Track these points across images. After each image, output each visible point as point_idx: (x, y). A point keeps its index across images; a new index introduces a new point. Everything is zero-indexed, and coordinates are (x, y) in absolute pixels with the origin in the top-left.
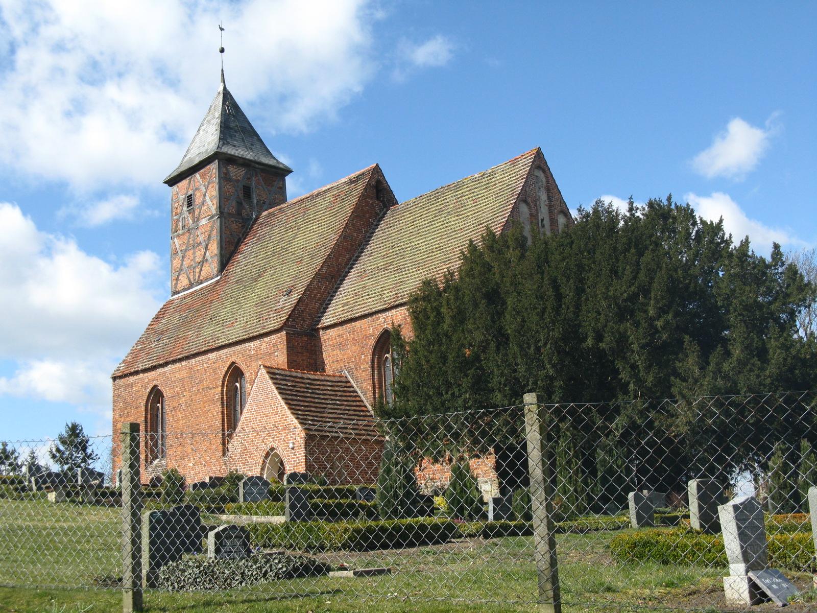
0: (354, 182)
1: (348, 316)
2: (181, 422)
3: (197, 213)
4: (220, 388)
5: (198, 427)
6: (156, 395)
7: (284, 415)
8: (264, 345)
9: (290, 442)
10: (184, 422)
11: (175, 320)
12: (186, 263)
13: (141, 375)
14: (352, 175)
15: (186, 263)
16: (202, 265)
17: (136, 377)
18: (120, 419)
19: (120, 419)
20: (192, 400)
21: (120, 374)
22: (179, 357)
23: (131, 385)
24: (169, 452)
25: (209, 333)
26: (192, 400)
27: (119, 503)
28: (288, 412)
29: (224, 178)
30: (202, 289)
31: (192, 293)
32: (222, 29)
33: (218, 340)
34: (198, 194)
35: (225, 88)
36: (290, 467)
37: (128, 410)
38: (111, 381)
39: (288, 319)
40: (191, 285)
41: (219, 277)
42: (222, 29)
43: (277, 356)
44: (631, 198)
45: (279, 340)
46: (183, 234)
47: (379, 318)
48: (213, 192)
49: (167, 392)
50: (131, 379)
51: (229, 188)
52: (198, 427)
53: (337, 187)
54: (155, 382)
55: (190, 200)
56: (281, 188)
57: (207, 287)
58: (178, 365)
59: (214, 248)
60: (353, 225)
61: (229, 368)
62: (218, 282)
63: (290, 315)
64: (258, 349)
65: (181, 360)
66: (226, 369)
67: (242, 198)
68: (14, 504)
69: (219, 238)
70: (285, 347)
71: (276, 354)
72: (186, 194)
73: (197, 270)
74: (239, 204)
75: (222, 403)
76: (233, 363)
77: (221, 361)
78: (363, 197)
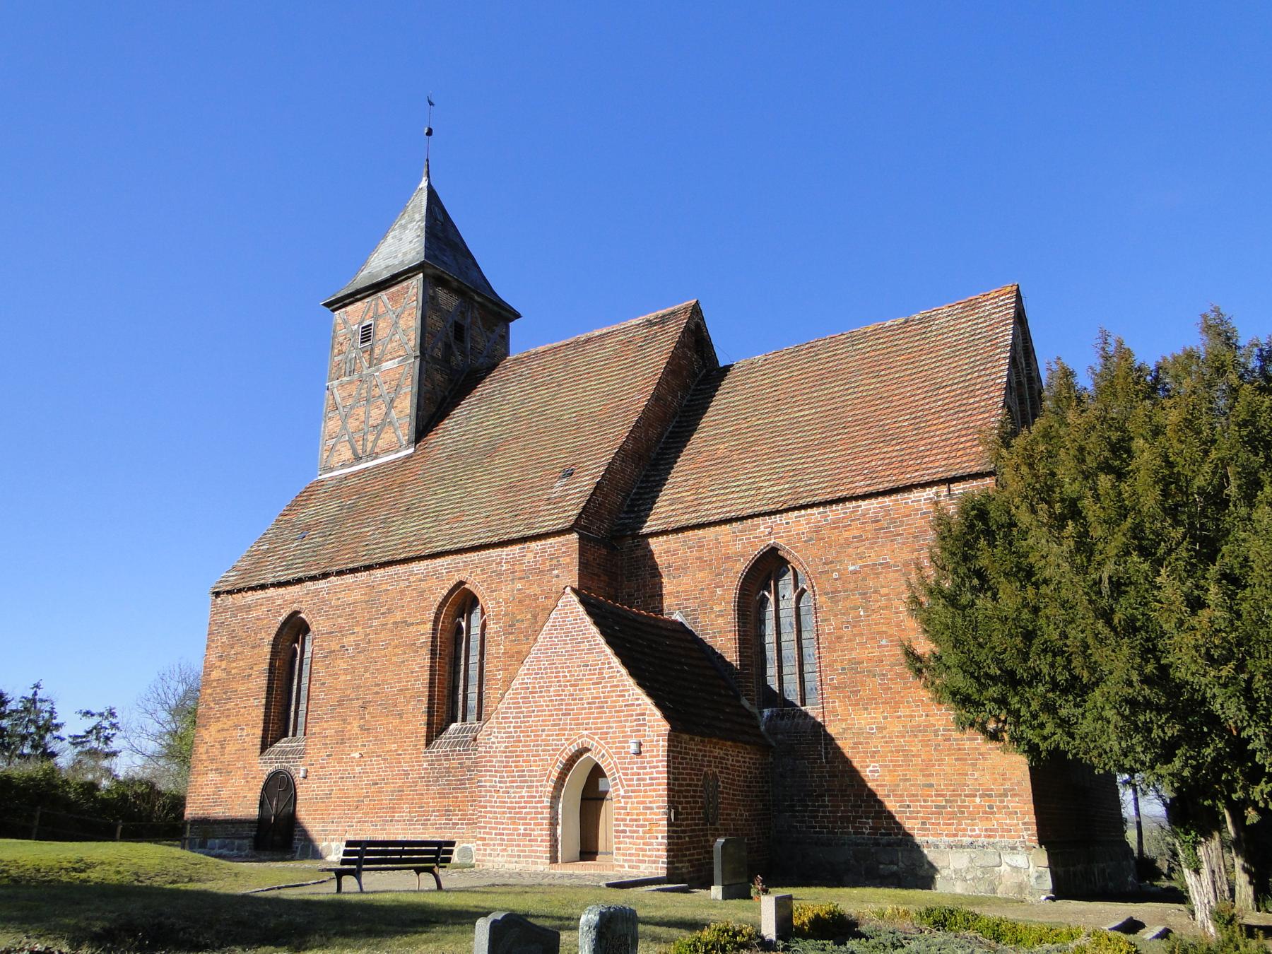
0: (655, 324)
1: (684, 520)
2: (342, 678)
3: (377, 351)
4: (430, 625)
5: (376, 689)
6: (295, 628)
7: (617, 686)
8: (530, 555)
9: (631, 740)
10: (349, 677)
11: (333, 507)
12: (352, 424)
13: (271, 591)
14: (651, 316)
15: (352, 424)
16: (382, 430)
17: (260, 594)
18: (218, 664)
19: (218, 664)
20: (369, 642)
21: (228, 588)
22: (351, 566)
23: (248, 608)
24: (314, 729)
25: (406, 533)
26: (369, 642)
27: (790, 898)
28: (630, 682)
29: (429, 304)
30: (378, 466)
31: (359, 472)
32: (431, 104)
33: (430, 542)
34: (382, 324)
35: (429, 184)
36: (626, 792)
37: (238, 648)
38: (211, 598)
39: (580, 514)
40: (358, 459)
41: (411, 450)
42: (431, 104)
43: (558, 576)
44: (37, 686)
45: (564, 549)
46: (351, 382)
47: (758, 525)
48: (410, 322)
49: (317, 624)
50: (251, 597)
51: (434, 319)
52: (376, 689)
53: (625, 331)
54: (295, 607)
55: (367, 334)
56: (503, 337)
57: (387, 463)
58: (349, 578)
59: (406, 405)
60: (667, 382)
61: (451, 592)
62: (409, 457)
63: (584, 507)
64: (514, 562)
65: (353, 571)
66: (445, 592)
67: (452, 339)
68: (329, 847)
69: (415, 389)
70: (576, 561)
71: (556, 572)
72: (359, 324)
73: (371, 438)
74: (447, 347)
75: (433, 652)
76: (462, 583)
77: (436, 579)
78: (681, 345)
